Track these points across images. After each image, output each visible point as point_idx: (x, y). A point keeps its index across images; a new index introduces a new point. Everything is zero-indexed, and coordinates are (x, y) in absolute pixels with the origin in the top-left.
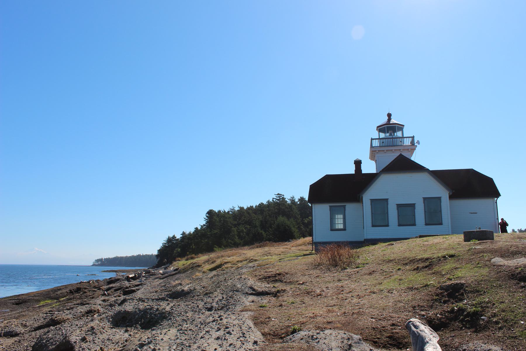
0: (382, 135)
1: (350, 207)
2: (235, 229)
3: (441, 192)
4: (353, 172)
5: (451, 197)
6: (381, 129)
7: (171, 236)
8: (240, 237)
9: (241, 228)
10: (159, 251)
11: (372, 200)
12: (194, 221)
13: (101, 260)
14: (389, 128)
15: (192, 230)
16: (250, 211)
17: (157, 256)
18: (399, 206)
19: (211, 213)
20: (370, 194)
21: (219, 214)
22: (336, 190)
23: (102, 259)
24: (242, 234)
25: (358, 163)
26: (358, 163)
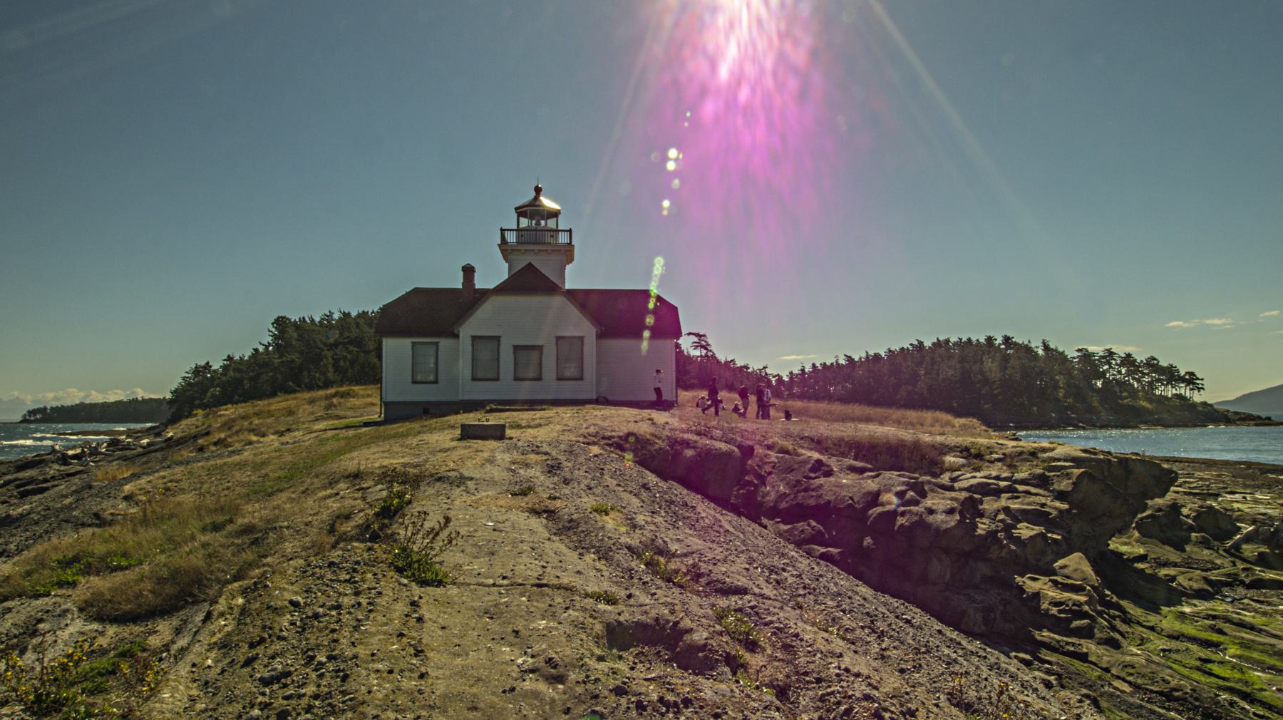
0: (524, 222)
1: (444, 343)
2: (330, 354)
3: (583, 328)
4: (458, 284)
5: (600, 336)
6: (521, 212)
7: (202, 363)
8: (336, 368)
9: (339, 351)
10: (175, 392)
11: (474, 338)
12: (249, 337)
13: (43, 410)
14: (530, 210)
15: (248, 354)
16: (361, 321)
17: (171, 402)
18: (517, 348)
19: (281, 322)
20: (478, 323)
21: (300, 326)
22: (430, 314)
23: (45, 408)
24: (342, 363)
25: (469, 271)
26: (469, 271)
